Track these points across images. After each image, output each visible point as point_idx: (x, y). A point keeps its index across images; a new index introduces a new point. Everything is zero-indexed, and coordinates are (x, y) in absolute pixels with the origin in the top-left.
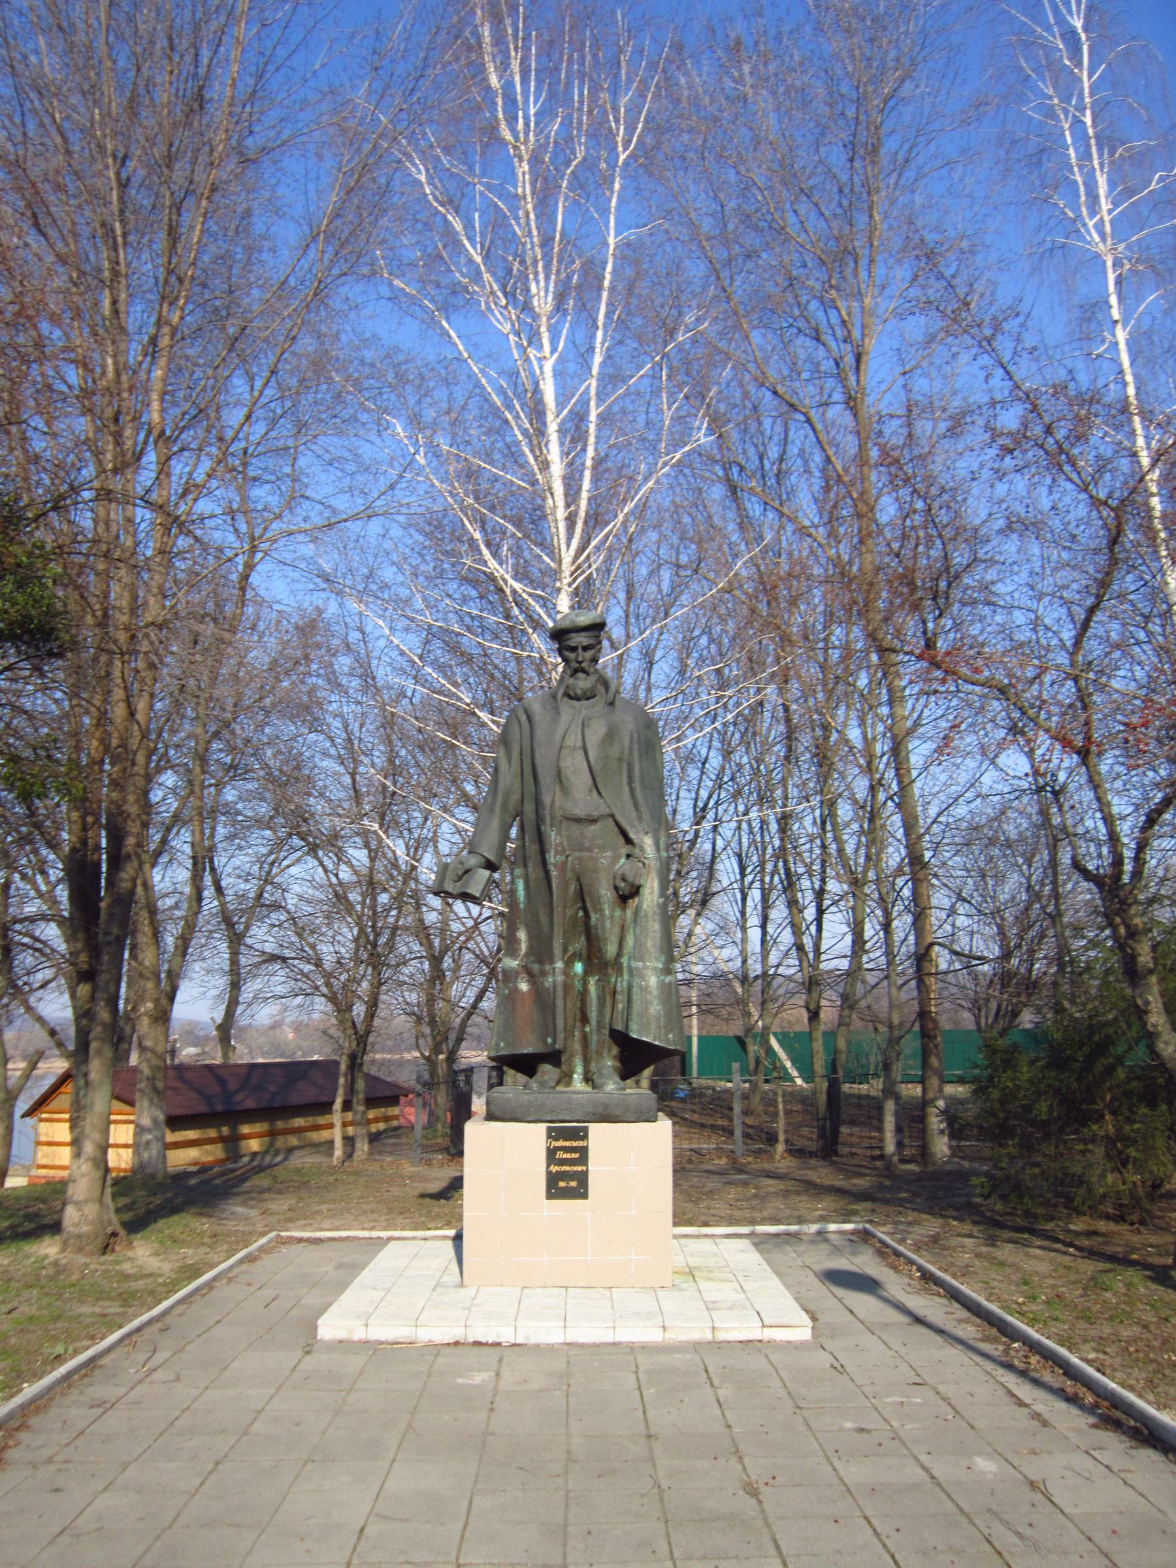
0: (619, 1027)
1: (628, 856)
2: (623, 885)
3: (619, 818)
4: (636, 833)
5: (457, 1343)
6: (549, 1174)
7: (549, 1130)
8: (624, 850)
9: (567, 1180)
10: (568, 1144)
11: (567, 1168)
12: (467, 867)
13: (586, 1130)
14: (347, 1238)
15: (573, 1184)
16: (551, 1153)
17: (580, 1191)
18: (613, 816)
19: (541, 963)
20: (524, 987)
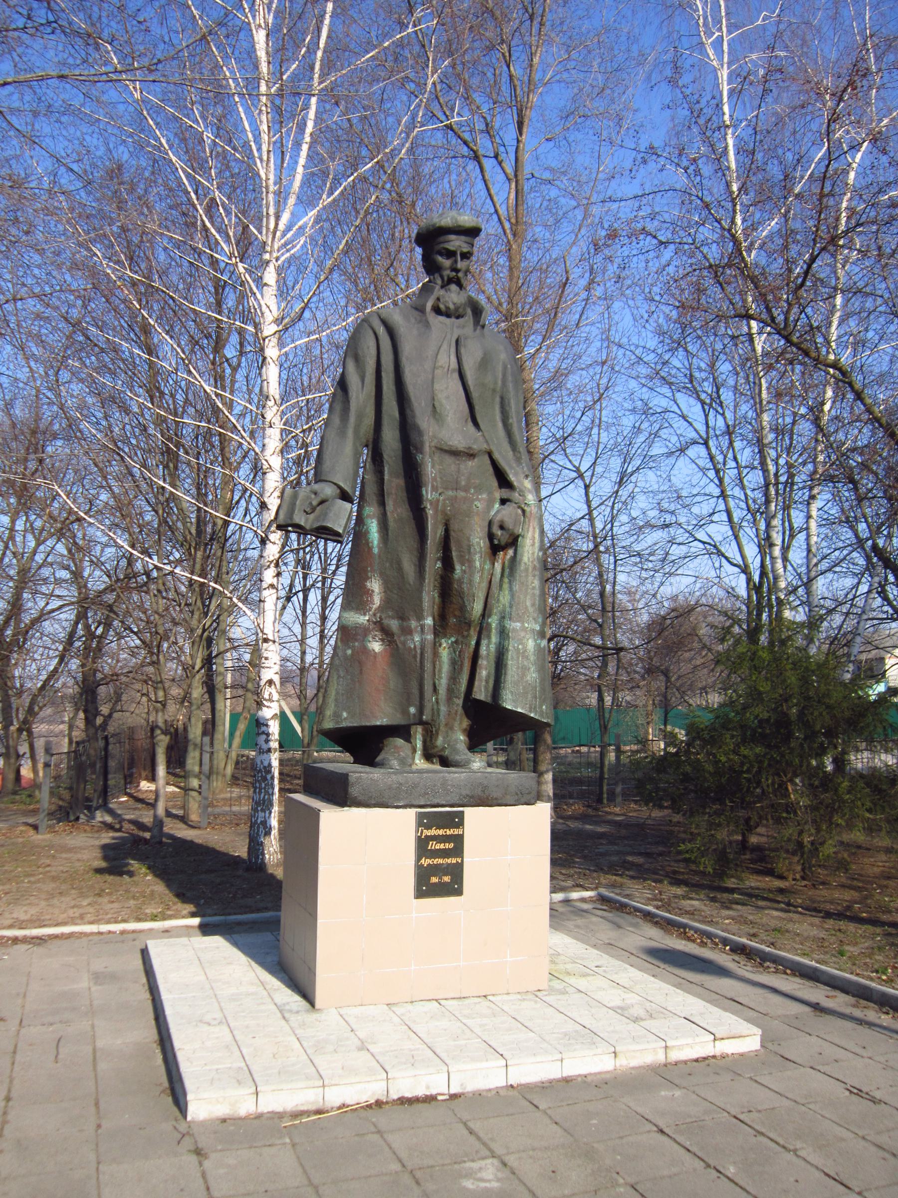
0: (481, 693)
1: (503, 502)
2: (499, 533)
3: (496, 456)
4: (516, 474)
5: (379, 1104)
6: (419, 868)
7: (420, 817)
8: (498, 494)
9: (439, 876)
10: (441, 832)
11: (440, 861)
12: (322, 496)
13: (461, 815)
14: (70, 935)
15: (447, 879)
16: (422, 846)
17: (454, 888)
18: (490, 454)
19: (402, 618)
20: (376, 646)
